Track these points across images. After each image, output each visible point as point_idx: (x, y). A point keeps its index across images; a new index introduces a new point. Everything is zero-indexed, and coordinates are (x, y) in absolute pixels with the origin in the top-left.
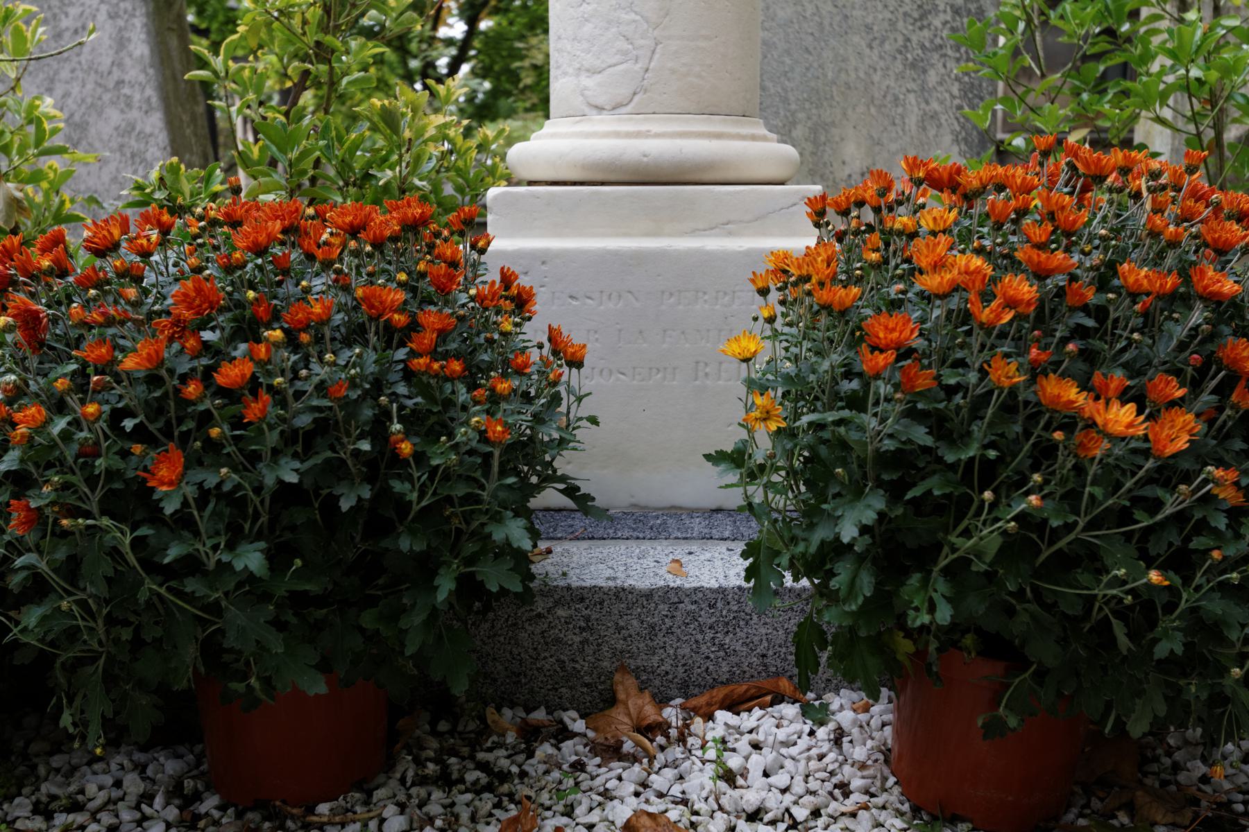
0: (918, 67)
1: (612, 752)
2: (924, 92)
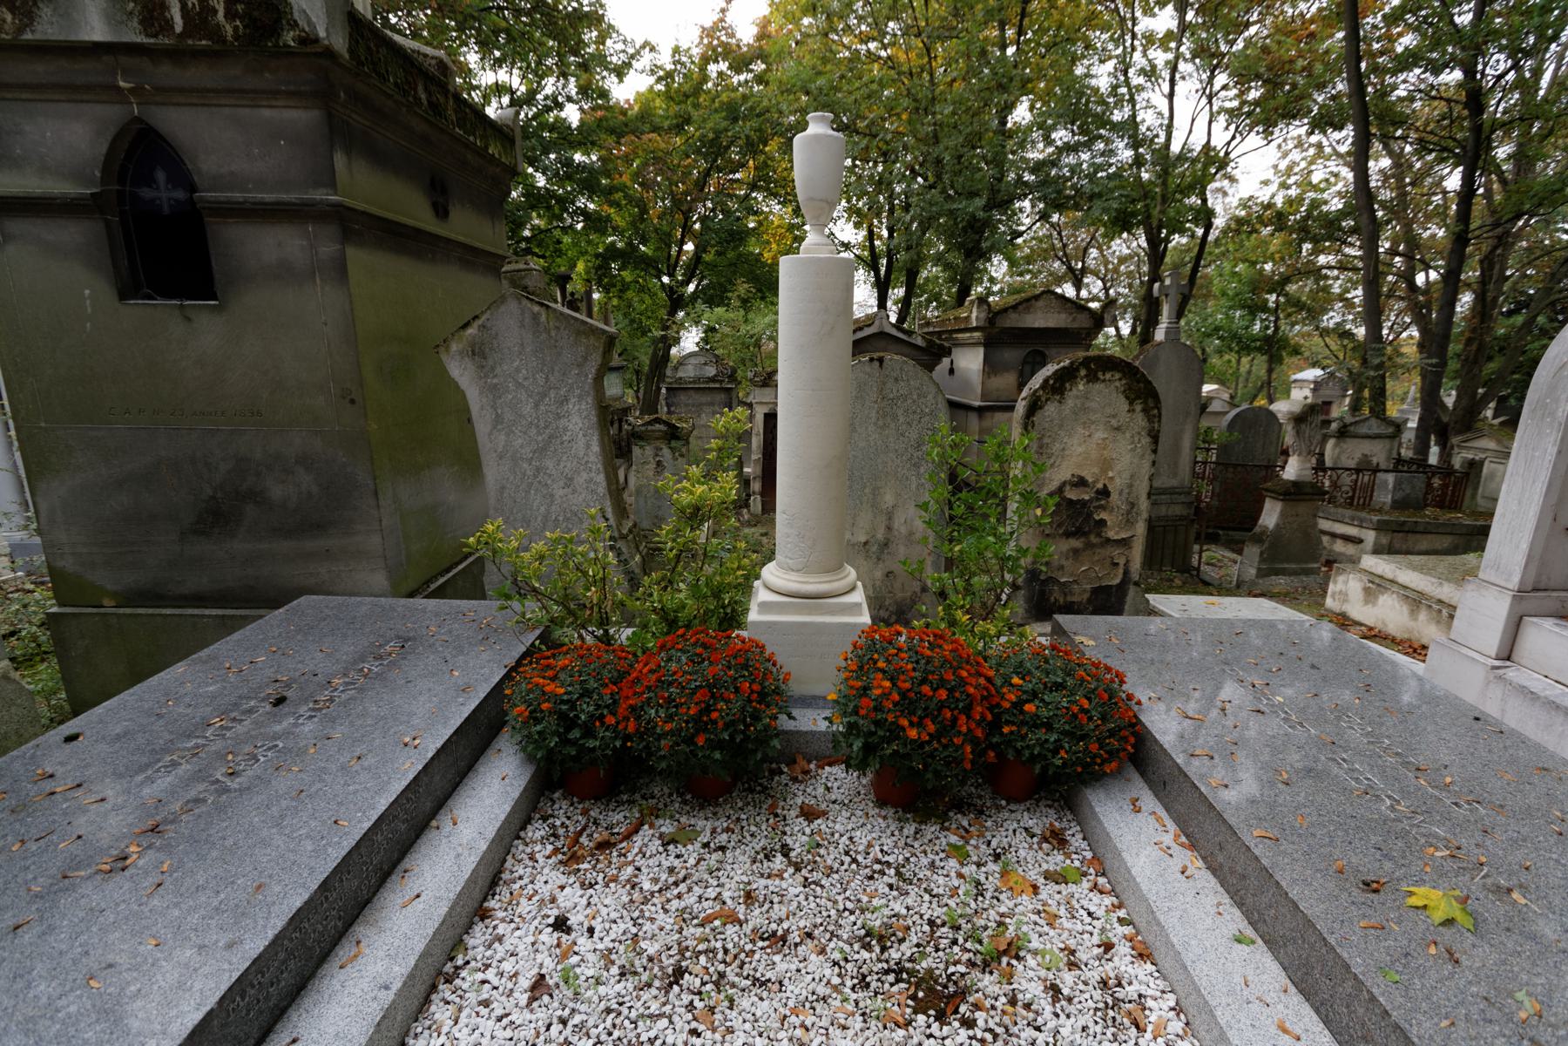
0: (917, 466)
1: (795, 780)
2: (919, 476)
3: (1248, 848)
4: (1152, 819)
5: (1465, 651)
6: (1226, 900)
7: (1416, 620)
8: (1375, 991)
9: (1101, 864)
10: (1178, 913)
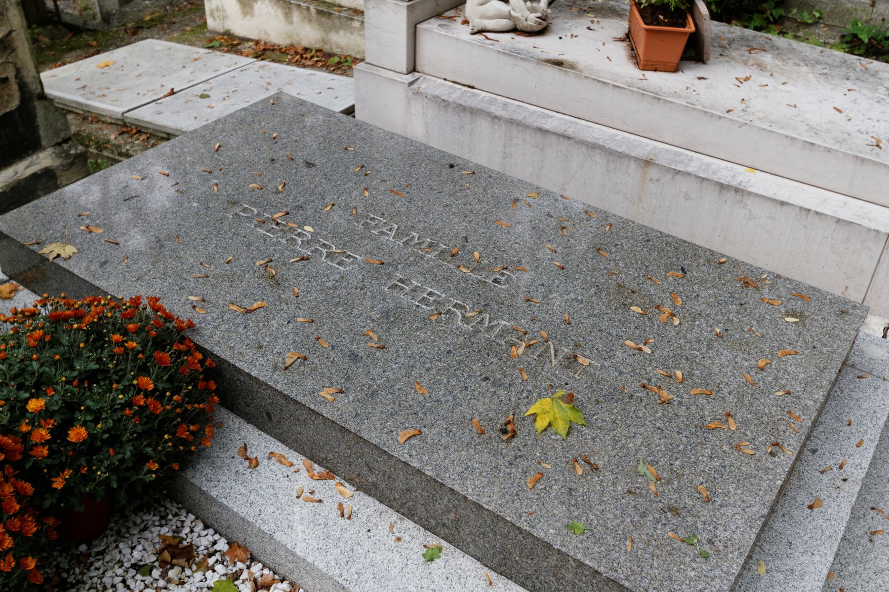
3: (406, 464)
4: (275, 465)
5: (383, 73)
6: (394, 516)
7: (291, 23)
8: (579, 557)
9: (245, 549)
10: (368, 574)
